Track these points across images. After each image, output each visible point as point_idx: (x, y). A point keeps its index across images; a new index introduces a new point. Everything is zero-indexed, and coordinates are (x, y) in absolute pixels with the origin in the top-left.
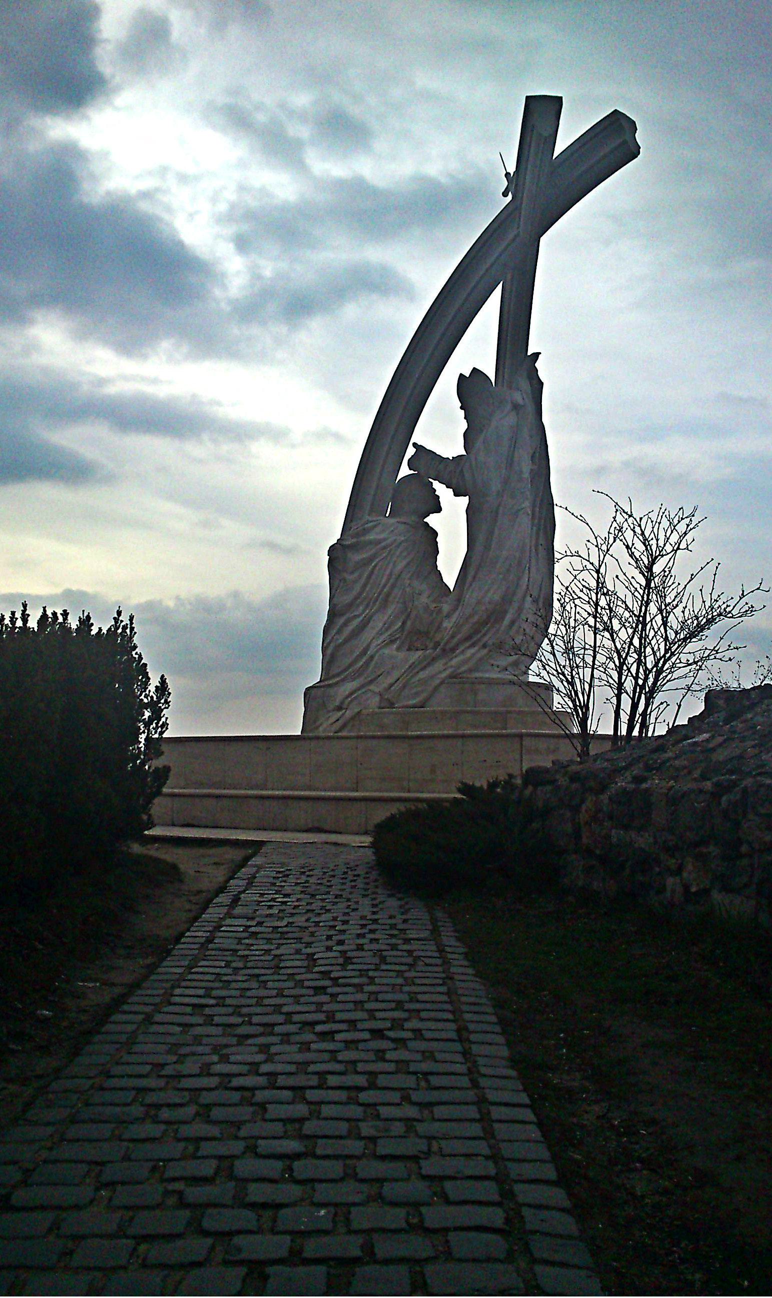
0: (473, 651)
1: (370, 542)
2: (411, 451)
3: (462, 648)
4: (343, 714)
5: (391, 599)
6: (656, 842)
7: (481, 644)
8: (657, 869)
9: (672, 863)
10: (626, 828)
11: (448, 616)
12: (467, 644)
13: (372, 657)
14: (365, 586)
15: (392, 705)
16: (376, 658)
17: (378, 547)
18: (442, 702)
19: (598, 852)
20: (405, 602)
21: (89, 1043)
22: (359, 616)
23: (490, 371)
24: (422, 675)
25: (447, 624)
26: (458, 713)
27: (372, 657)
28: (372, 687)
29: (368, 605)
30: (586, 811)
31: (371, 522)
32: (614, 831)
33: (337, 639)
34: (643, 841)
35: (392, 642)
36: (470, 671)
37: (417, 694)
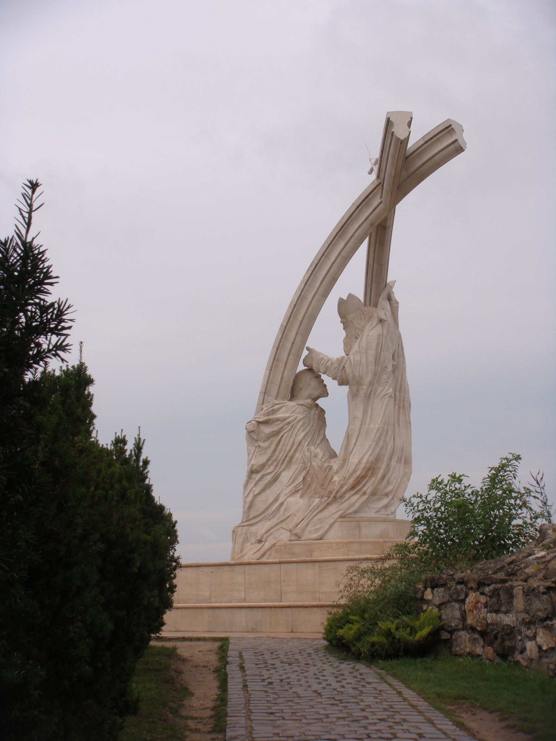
0: (356, 497)
1: (278, 420)
2: (305, 353)
3: (348, 495)
4: (263, 546)
5: (294, 460)
6: (517, 620)
7: (361, 492)
8: (519, 638)
9: (529, 633)
10: (497, 611)
11: (337, 472)
12: (352, 492)
13: (282, 504)
14: (274, 451)
15: (298, 537)
16: (285, 504)
17: (284, 423)
18: (334, 536)
19: (479, 629)
20: (304, 463)
21: (212, 728)
22: (270, 473)
23: (361, 296)
24: (321, 516)
25: (336, 478)
26: (349, 543)
27: (282, 504)
28: (283, 525)
29: (277, 466)
30: (469, 603)
31: (278, 404)
32: (488, 614)
33: (254, 491)
34: (508, 619)
35: (297, 491)
36: (355, 512)
37: (317, 530)
